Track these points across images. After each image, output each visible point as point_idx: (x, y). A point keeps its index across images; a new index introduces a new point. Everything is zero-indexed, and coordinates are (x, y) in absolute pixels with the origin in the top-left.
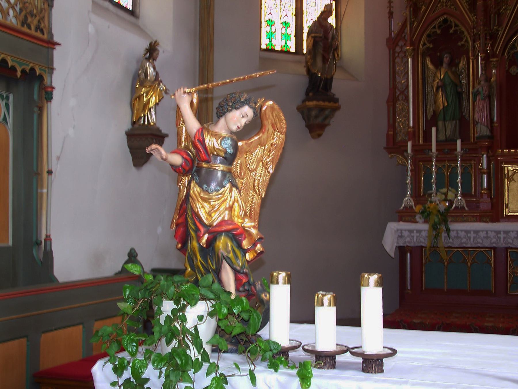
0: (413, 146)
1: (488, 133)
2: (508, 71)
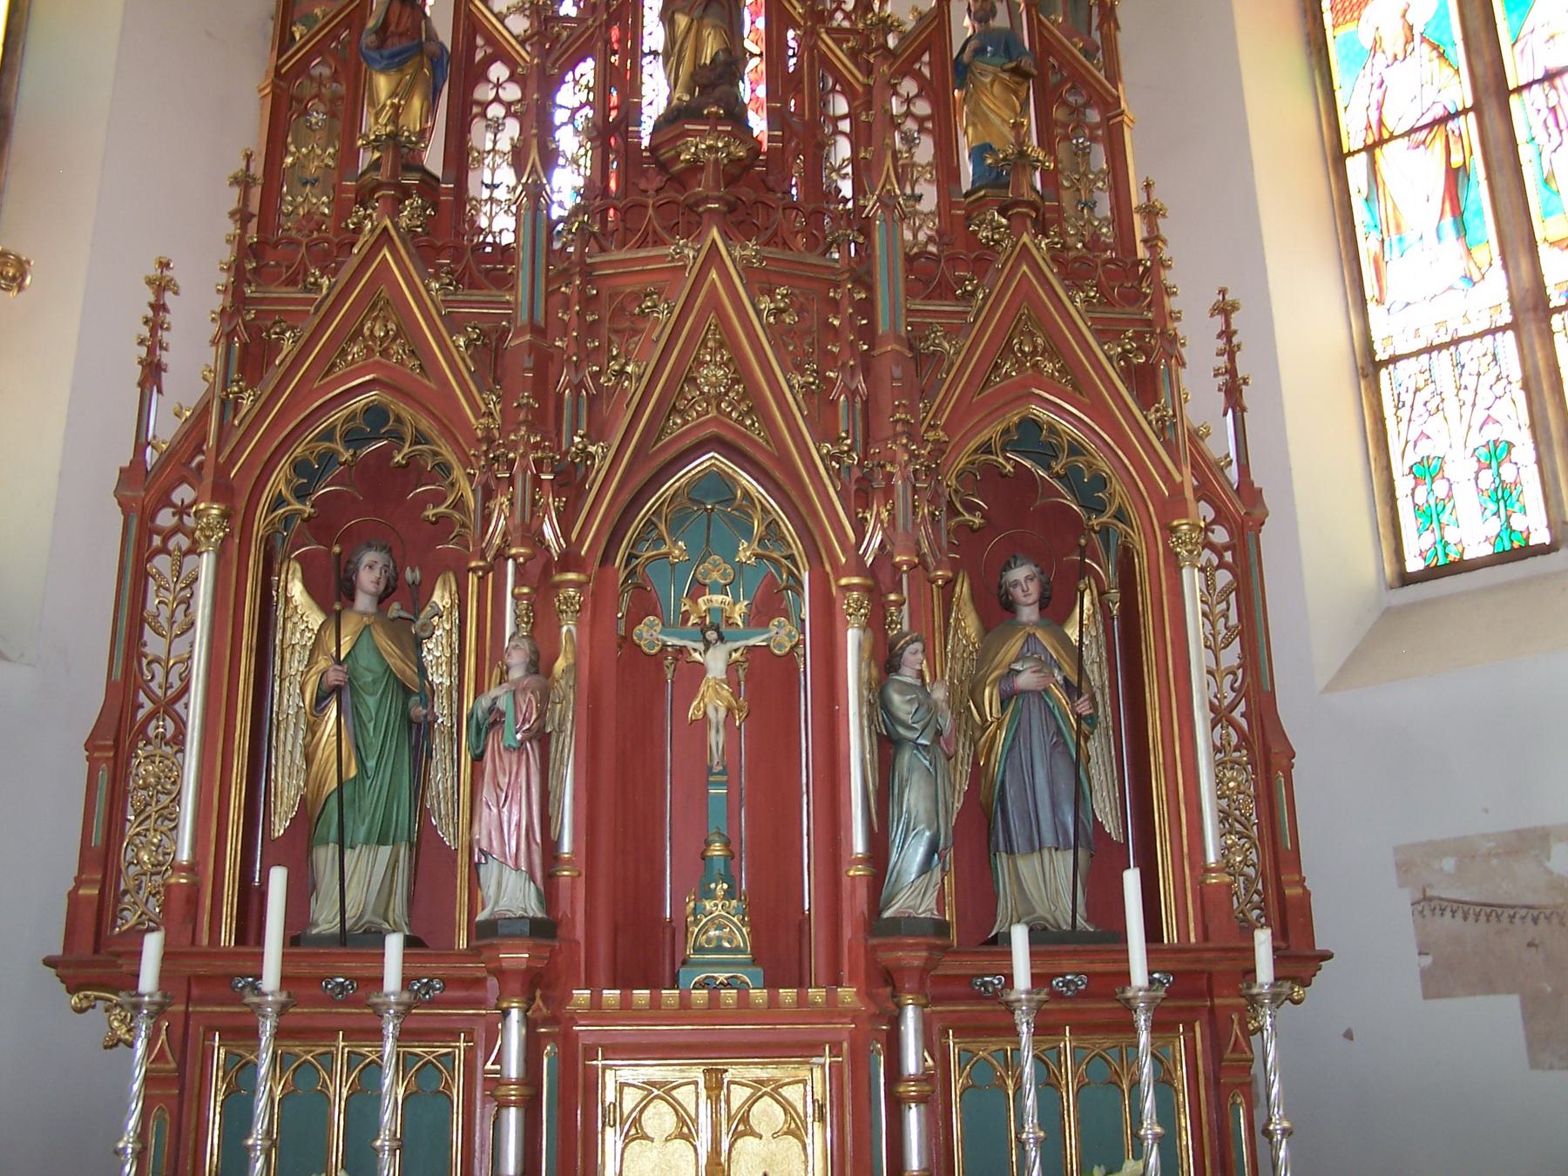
0: (168, 956)
1: (534, 909)
2: (627, 640)
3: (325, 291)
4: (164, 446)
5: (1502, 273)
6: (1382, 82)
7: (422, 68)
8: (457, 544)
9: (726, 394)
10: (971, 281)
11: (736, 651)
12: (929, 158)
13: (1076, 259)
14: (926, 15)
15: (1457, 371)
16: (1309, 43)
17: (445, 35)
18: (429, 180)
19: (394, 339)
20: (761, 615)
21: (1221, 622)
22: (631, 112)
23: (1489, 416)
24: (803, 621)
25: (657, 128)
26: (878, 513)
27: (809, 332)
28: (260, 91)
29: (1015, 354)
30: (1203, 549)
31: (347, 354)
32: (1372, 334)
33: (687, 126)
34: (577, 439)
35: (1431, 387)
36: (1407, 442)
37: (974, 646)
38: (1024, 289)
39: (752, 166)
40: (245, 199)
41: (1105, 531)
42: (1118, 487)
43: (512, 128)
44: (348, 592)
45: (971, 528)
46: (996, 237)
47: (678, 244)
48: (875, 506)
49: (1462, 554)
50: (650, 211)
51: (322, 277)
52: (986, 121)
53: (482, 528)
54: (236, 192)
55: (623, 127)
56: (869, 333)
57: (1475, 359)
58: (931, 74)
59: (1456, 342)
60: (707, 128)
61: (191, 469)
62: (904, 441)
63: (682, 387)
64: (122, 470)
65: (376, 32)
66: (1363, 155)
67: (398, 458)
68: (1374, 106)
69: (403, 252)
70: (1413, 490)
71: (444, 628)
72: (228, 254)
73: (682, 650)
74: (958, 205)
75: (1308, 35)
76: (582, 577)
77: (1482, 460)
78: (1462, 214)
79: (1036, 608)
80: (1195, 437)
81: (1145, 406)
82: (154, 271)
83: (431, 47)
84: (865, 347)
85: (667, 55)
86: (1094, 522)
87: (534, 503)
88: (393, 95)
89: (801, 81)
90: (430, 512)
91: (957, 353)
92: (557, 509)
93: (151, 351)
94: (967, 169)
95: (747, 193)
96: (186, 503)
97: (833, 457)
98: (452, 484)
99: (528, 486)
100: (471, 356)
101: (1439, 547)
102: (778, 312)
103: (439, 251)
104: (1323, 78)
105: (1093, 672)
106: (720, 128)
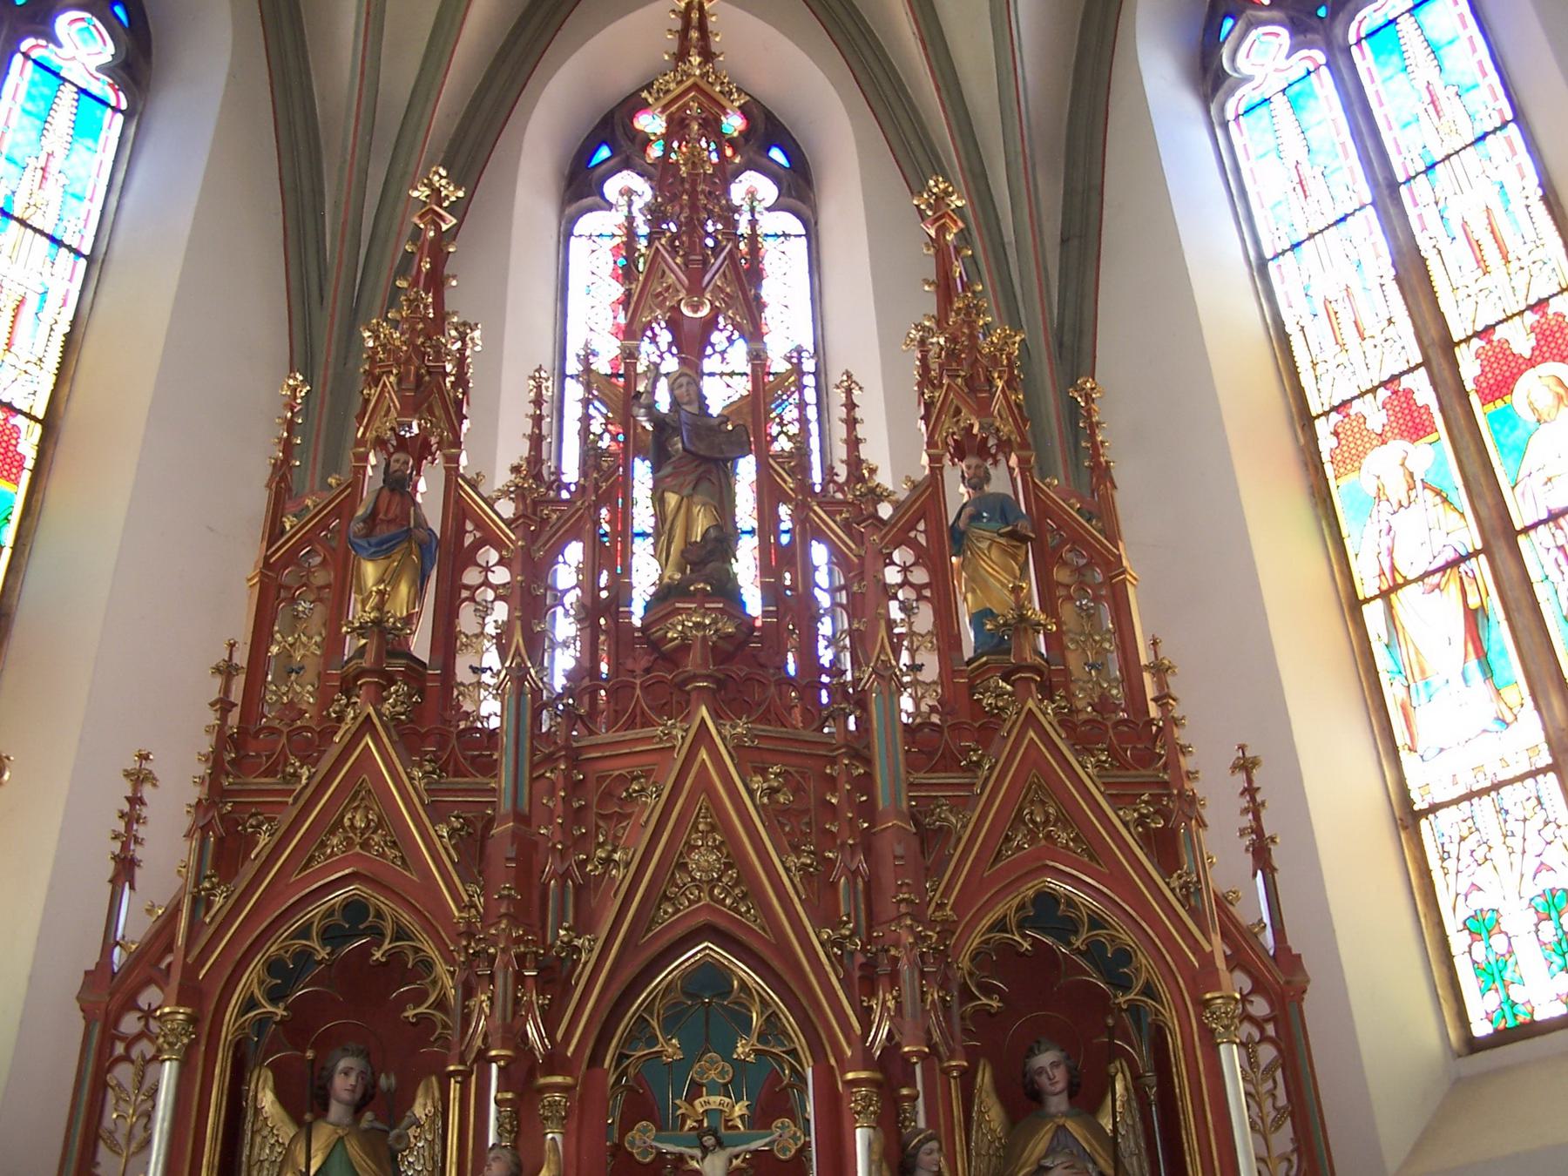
2: (619, 1147)
3: (304, 781)
4: (134, 947)
5: (1535, 713)
6: (1390, 529)
7: (411, 553)
8: (441, 1047)
9: (719, 879)
10: (975, 751)
11: (737, 1157)
12: (930, 627)
13: (1086, 722)
14: (920, 483)
15: (1501, 817)
16: (1313, 495)
17: (435, 522)
18: (415, 669)
19: (374, 832)
20: (760, 1119)
21: (1268, 1104)
22: (622, 590)
23: (1542, 863)
24: (808, 1121)
25: (647, 608)
26: (884, 1002)
27: (807, 811)
28: (249, 580)
29: (1026, 824)
30: (1241, 1022)
31: (326, 846)
32: (1408, 782)
33: (678, 605)
34: (562, 932)
35: (1476, 836)
36: (1457, 895)
37: (1000, 1143)
38: (1033, 759)
39: (746, 642)
40: (226, 689)
41: (1135, 1009)
42: (1144, 961)
43: (501, 611)
44: (321, 1102)
45: (990, 1014)
46: (1000, 704)
47: (665, 725)
48: (881, 993)
49: (1532, 1014)
50: (638, 692)
51: (301, 767)
52: (985, 587)
53: (462, 1028)
54: (218, 681)
55: (614, 607)
56: (868, 811)
57: (1519, 804)
58: (927, 541)
59: (1496, 787)
60: (693, 606)
61: (160, 969)
62: (909, 922)
63: (673, 873)
64: (87, 973)
65: (364, 521)
66: (1379, 601)
67: (378, 955)
68: (1385, 553)
69: (386, 740)
70: (1470, 946)
71: (426, 1139)
72: (207, 744)
73: (680, 1158)
74: (960, 673)
75: (1312, 487)
76: (569, 1080)
77: (1540, 910)
78: (1486, 655)
79: (1065, 1096)
80: (1222, 902)
81: (1167, 872)
82: (132, 764)
83: (421, 534)
84: (866, 825)
85: (658, 532)
86: (1121, 1000)
87: (517, 1001)
88: (380, 581)
89: (794, 555)
90: (410, 1013)
91: (964, 826)
92: (541, 1007)
93: (125, 846)
94: (969, 636)
95: (739, 670)
96: (153, 1007)
97: (835, 943)
98: (434, 982)
99: (510, 981)
100: (455, 847)
101: (1506, 1007)
102: (772, 792)
103: (424, 738)
104: (1330, 526)
105: (1132, 1165)
106: (707, 605)
